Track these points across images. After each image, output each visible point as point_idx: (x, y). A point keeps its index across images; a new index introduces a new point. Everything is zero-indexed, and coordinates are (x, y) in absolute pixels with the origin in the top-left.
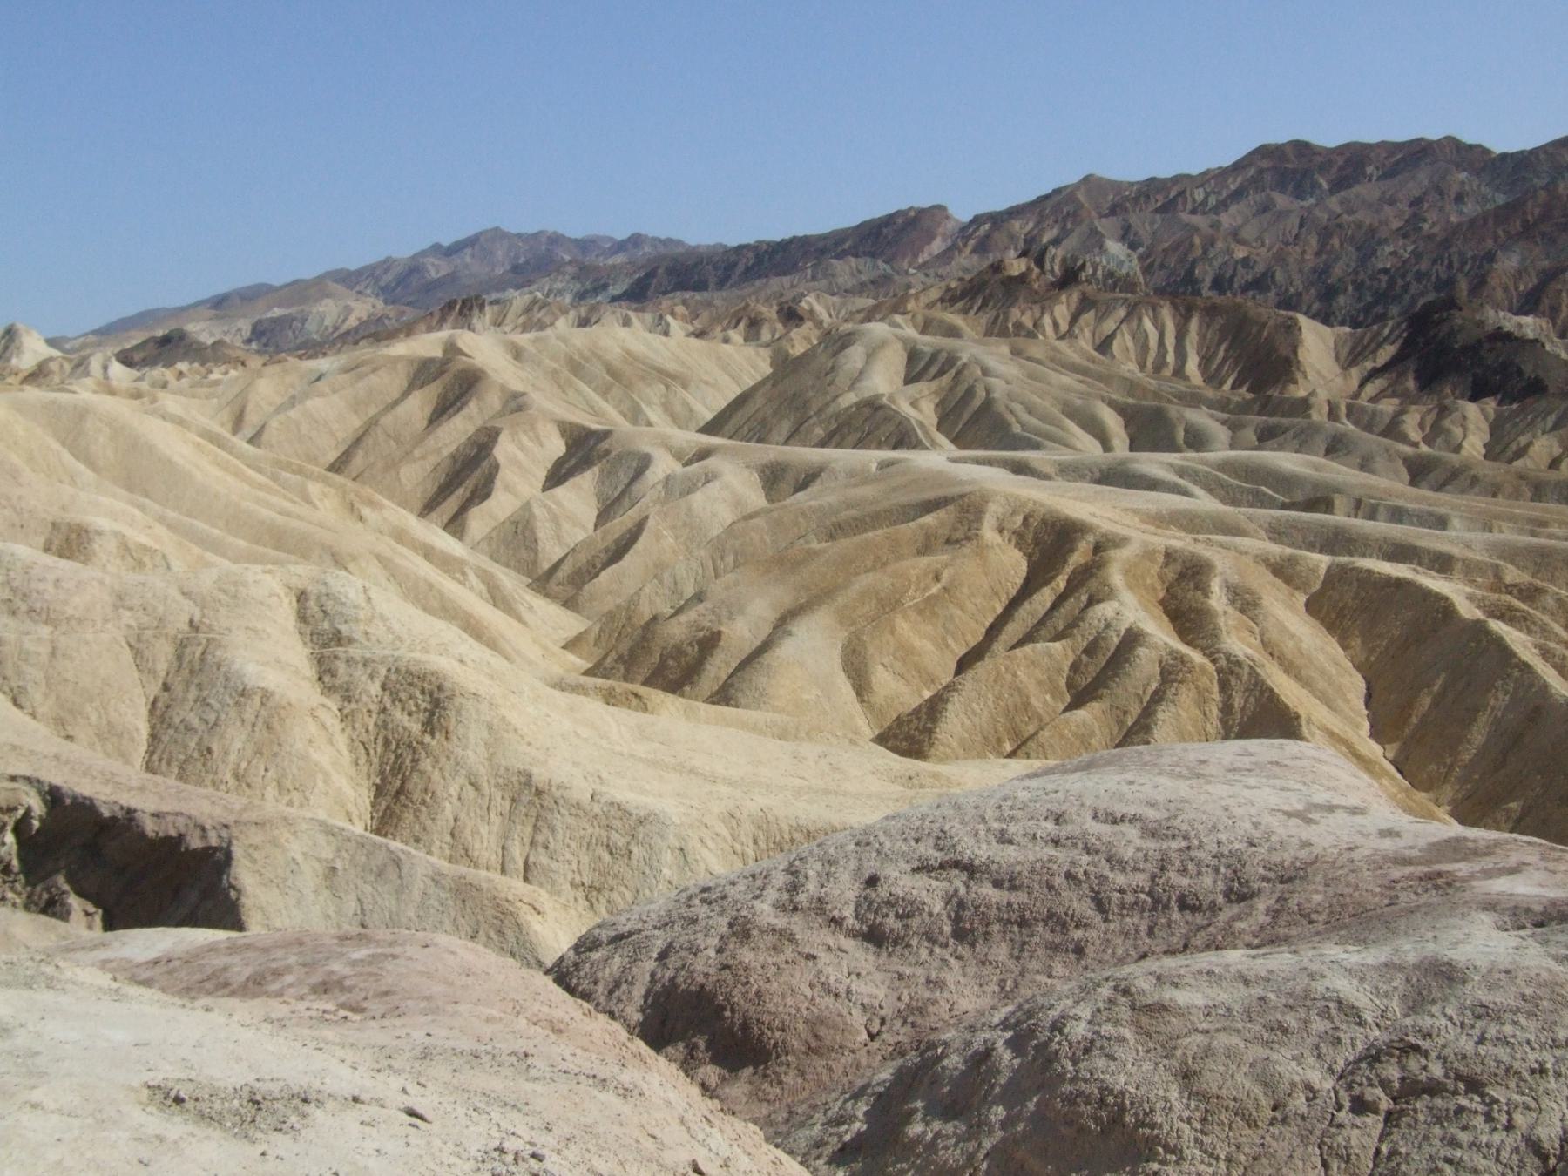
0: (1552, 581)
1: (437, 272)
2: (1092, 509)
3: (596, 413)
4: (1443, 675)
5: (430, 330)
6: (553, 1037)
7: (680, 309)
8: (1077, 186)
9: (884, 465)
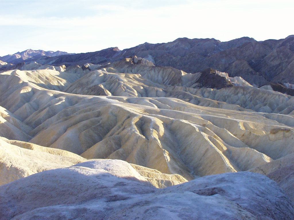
1: (18, 57)
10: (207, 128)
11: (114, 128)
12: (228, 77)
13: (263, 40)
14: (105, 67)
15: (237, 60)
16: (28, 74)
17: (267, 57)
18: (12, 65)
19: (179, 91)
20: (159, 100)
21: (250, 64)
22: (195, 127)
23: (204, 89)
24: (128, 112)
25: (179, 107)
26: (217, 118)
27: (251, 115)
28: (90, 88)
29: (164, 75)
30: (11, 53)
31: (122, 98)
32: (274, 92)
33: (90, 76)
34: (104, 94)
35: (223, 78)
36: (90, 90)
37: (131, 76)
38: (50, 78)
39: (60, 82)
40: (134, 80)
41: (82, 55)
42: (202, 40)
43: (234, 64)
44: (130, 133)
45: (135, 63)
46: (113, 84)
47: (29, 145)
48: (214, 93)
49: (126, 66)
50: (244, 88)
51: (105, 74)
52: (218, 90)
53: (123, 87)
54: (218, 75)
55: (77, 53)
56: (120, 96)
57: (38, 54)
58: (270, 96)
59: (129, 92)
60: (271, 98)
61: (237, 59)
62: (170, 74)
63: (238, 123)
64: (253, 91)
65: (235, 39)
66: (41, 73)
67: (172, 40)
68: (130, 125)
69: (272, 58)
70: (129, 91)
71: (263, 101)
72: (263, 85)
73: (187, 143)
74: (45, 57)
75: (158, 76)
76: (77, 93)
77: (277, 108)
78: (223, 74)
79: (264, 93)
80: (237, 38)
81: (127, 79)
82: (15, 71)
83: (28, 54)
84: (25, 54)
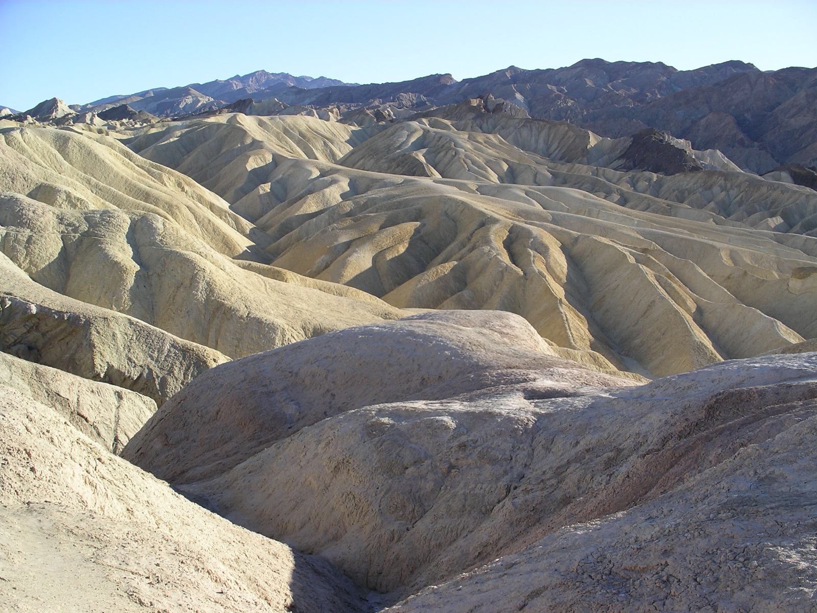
0: (664, 208)
1: (237, 87)
2: (485, 206)
3: (292, 151)
4: (644, 382)
5: (229, 112)
6: (33, 454)
7: (335, 110)
8: (506, 70)
9: (406, 181)
10: (651, 257)
11: (452, 245)
12: (690, 150)
13: (776, 68)
14: (425, 116)
15: (712, 113)
16: (261, 124)
17: (780, 107)
18: (224, 103)
19: (583, 174)
20: (545, 192)
21: (740, 123)
22: (627, 254)
23: (639, 174)
24: (482, 214)
25: (588, 209)
26: (671, 237)
27: (743, 235)
28: (394, 160)
29: (550, 140)
31: (465, 184)
32: (795, 187)
33: (393, 134)
34: (424, 174)
35: (681, 152)
36: (394, 164)
37: (481, 137)
38: (309, 135)
39: (330, 144)
40: (486, 147)
41: (374, 86)
42: (637, 65)
43: (703, 121)
44: (486, 258)
45: (488, 111)
46: (442, 154)
47: (279, 272)
48: (659, 184)
49: (471, 116)
50: (727, 176)
51: (426, 132)
52: (669, 178)
53: (464, 160)
54: (668, 144)
55: (362, 84)
56: (461, 179)
57: (280, 81)
58: (786, 195)
59: (476, 172)
60: (788, 200)
61: (711, 111)
62: (563, 138)
63: (719, 250)
64: (747, 183)
65: (710, 65)
66: (289, 122)
67: (568, 63)
68: (487, 242)
69: (794, 111)
70: (477, 169)
71: (768, 206)
72: (770, 170)
73: (608, 286)
74: (294, 90)
75: (537, 141)
76: (366, 168)
77: (800, 223)
78: (681, 143)
79: (772, 187)
80: (715, 63)
81: (472, 144)
82: (235, 115)
83: (258, 81)
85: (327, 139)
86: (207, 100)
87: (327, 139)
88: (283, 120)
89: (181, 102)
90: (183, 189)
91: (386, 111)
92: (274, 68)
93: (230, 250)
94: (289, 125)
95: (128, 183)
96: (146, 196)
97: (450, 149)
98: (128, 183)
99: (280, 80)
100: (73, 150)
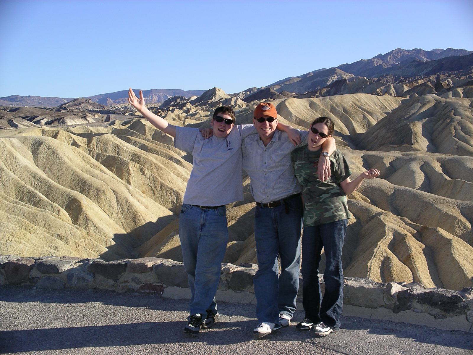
1: (377, 64)
30: (367, 57)
38: (351, 110)
83: (395, 57)
84: (390, 58)
85: (368, 112)
86: (349, 77)
87: (368, 112)
88: (331, 100)
89: (328, 80)
90: (143, 174)
91: (446, 82)
92: (408, 45)
93: (136, 224)
94: (336, 105)
95: (75, 174)
96: (83, 184)
97: (449, 117)
98: (75, 174)
99: (413, 54)
100: (42, 152)
